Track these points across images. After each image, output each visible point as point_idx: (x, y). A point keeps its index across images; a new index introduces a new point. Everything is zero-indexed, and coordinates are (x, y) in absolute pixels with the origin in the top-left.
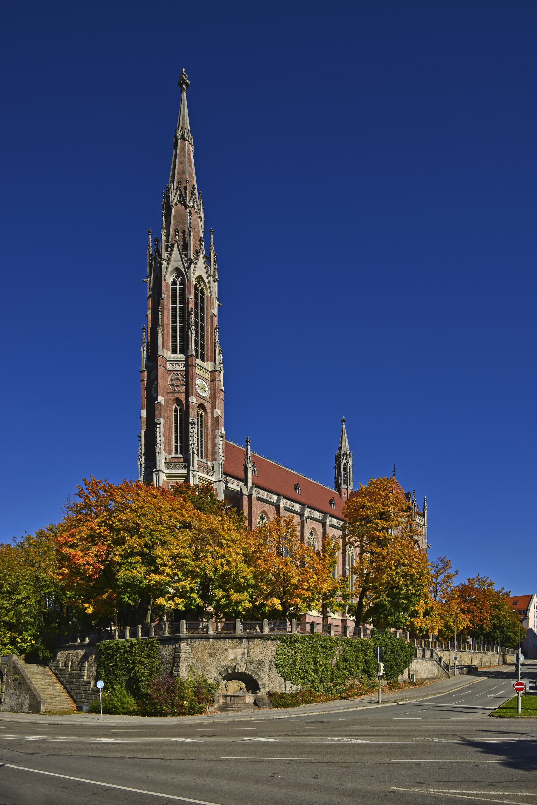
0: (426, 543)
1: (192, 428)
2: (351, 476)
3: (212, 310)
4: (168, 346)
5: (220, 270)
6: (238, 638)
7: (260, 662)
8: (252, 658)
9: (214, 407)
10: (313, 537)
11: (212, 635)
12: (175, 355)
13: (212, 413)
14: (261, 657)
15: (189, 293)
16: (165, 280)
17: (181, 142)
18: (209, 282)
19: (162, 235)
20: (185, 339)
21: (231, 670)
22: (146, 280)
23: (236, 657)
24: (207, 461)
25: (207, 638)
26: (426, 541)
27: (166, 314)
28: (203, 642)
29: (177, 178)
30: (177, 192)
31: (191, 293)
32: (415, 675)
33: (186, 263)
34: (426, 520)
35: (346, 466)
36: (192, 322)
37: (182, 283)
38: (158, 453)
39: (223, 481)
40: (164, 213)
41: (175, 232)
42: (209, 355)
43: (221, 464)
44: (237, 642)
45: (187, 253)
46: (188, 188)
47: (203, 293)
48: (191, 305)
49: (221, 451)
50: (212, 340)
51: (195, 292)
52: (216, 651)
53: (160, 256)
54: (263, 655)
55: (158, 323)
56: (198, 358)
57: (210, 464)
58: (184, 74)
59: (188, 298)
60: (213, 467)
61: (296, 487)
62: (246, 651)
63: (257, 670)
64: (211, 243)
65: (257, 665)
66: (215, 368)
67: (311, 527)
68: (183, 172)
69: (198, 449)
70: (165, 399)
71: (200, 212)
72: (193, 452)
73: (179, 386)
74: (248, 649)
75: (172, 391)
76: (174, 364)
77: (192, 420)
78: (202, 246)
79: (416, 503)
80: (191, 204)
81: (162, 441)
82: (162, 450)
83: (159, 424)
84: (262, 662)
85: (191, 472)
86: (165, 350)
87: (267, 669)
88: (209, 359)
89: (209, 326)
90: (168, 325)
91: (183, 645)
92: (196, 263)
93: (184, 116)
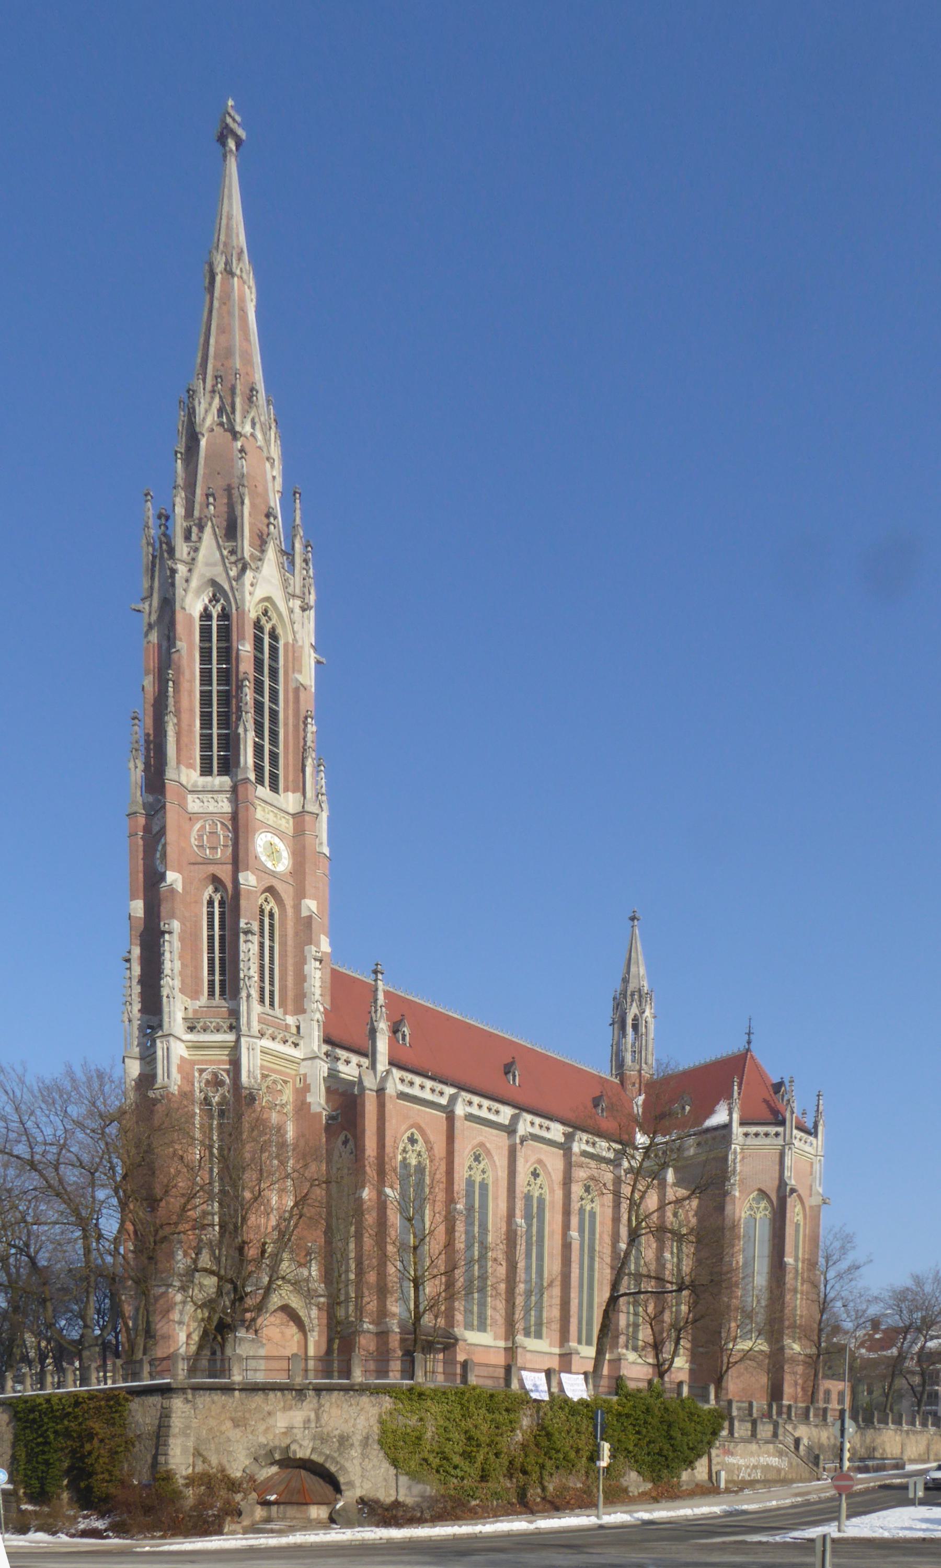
0: (819, 1194)
1: (246, 942)
2: (650, 1042)
3: (297, 676)
4: (191, 758)
5: (321, 583)
6: (296, 1390)
7: (344, 1441)
8: (325, 1431)
9: (300, 894)
10: (539, 1181)
11: (239, 1384)
12: (209, 779)
13: (297, 907)
14: (346, 1428)
15: (241, 638)
16: (183, 608)
17: (222, 279)
18: (291, 611)
19: (174, 505)
20: (230, 743)
21: (281, 1454)
22: (140, 606)
23: (290, 1428)
24: (285, 1013)
25: (227, 1389)
26: (821, 1190)
27: (185, 685)
28: (218, 1397)
29: (214, 367)
30: (212, 398)
31: (244, 639)
32: (723, 1473)
33: (234, 569)
34: (820, 1143)
35: (637, 1020)
36: (246, 704)
37: (225, 615)
38: (168, 997)
39: (321, 1059)
40: (181, 453)
41: (207, 496)
42: (291, 778)
43: (318, 1021)
44: (294, 1398)
45: (236, 546)
46: (238, 391)
47: (274, 636)
48: (246, 666)
49: (318, 991)
50: (296, 744)
51: (256, 636)
52: (247, 1415)
53: (171, 551)
54: (351, 1424)
55: (166, 707)
56: (263, 785)
57: (291, 1020)
58: (230, 116)
59: (238, 650)
60: (298, 1027)
61: (508, 1069)
62: (313, 1415)
63: (336, 1455)
64: (295, 520)
65: (337, 1444)
66: (303, 807)
67: (533, 1159)
68: (228, 353)
69: (262, 990)
70: (183, 878)
71: (268, 446)
72: (249, 996)
73: (216, 848)
74: (317, 1412)
75: (199, 860)
76: (205, 800)
77: (246, 924)
78: (272, 527)
79: (795, 1105)
80: (248, 429)
81: (176, 971)
82: (177, 989)
83: (170, 933)
84: (348, 1437)
85: (243, 1040)
86: (183, 768)
87: (359, 1451)
88: (291, 785)
89: (291, 712)
90: (192, 710)
91: (177, 1404)
92: (258, 568)
93: (230, 218)
